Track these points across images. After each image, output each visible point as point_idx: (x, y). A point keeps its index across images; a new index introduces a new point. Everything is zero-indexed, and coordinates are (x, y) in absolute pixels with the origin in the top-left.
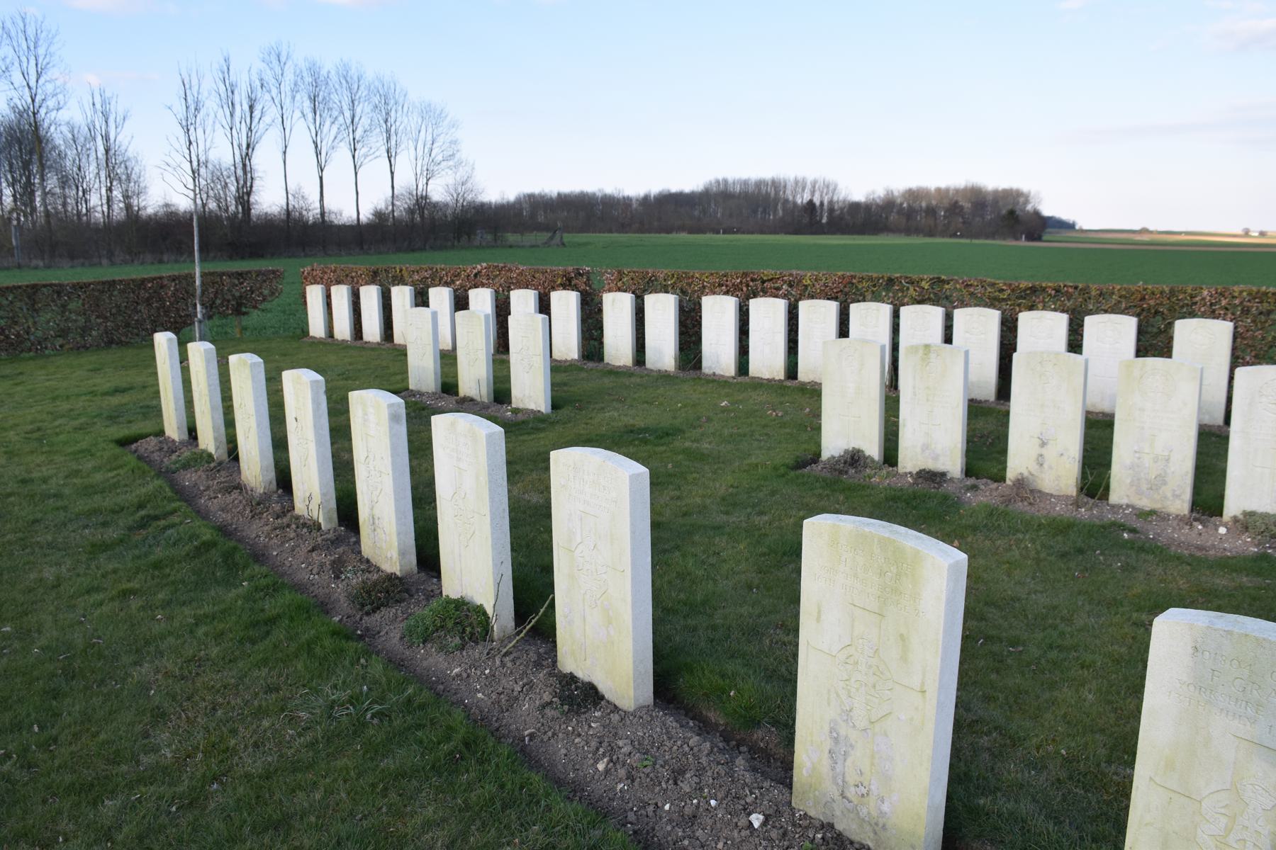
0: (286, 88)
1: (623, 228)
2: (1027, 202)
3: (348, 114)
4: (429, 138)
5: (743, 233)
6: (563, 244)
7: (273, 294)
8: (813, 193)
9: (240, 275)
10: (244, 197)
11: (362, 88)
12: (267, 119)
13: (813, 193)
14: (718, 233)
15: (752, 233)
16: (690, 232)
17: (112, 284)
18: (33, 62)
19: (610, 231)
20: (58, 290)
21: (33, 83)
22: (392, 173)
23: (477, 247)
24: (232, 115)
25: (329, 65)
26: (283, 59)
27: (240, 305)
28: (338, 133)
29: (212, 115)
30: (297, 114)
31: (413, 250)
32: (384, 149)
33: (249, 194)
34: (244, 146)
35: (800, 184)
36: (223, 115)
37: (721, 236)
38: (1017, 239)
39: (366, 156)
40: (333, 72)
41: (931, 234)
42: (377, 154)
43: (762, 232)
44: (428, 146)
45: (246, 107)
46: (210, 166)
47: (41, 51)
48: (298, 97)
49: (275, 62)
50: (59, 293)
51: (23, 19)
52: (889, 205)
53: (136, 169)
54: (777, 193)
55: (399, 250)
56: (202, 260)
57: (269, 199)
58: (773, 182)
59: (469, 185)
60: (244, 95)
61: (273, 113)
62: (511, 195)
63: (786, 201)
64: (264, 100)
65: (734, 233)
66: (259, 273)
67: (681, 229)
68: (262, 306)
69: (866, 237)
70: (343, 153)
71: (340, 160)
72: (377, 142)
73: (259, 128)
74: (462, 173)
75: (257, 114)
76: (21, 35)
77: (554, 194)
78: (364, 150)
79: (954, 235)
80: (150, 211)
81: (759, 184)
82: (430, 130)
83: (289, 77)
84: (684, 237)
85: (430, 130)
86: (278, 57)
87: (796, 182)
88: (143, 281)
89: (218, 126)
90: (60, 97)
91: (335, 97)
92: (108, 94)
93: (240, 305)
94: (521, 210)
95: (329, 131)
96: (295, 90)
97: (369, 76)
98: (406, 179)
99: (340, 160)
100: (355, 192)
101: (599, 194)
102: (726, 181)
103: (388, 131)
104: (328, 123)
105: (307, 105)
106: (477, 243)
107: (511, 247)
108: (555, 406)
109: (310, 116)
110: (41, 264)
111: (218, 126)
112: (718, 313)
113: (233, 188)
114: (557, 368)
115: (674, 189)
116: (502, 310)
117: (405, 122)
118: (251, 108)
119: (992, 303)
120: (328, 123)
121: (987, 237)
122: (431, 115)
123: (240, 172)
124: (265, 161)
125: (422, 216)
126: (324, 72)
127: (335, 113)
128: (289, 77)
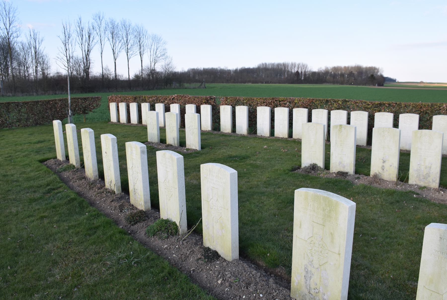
0: (102, 29)
1: (228, 81)
2: (378, 72)
3: (125, 39)
4: (156, 48)
5: (272, 83)
6: (205, 87)
7: (97, 106)
8: (298, 68)
9: (85, 99)
10: (87, 70)
11: (130, 29)
12: (95, 41)
13: (298, 68)
14: (263, 83)
15: (276, 83)
16: (253, 83)
17: (38, 102)
18: (8, 20)
19: (223, 83)
20: (17, 104)
21: (8, 27)
22: (142, 61)
23: (173, 89)
24: (82, 39)
25: (118, 20)
26: (101, 18)
27: (85, 110)
28: (121, 46)
29: (75, 39)
30: (106, 39)
31: (149, 90)
32: (139, 52)
33: (88, 69)
34: (87, 51)
35: (293, 65)
36: (79, 39)
37: (264, 84)
38: (374, 85)
39: (132, 55)
40: (120, 23)
41: (342, 83)
42: (136, 54)
43: (279, 83)
44: (155, 51)
45: (87, 36)
46: (74, 58)
47: (11, 15)
48: (107, 33)
49: (98, 19)
50: (17, 106)
51: (4, 4)
52: (327, 73)
53: (46, 59)
54: (285, 68)
55: (144, 89)
56: (71, 93)
57: (96, 71)
58: (284, 64)
59: (170, 65)
60: (87, 32)
61: (97, 38)
62: (186, 70)
63: (288, 71)
64: (94, 34)
65: (269, 83)
66: (92, 98)
67: (249, 82)
68: (93, 111)
69: (318, 85)
70: (124, 53)
71: (122, 56)
72: (136, 49)
73: (92, 44)
74: (168, 61)
75: (91, 39)
76: (3, 9)
77: (202, 69)
78: (131, 52)
79: (351, 84)
80: (51, 75)
81: (278, 65)
82: (156, 45)
83: (103, 25)
84: (250, 84)
85: (156, 45)
86: (99, 18)
87: (292, 64)
88: (49, 101)
89: (77, 43)
90: (18, 33)
91: (120, 33)
92: (36, 31)
93: (85, 110)
94: (190, 74)
95: (118, 45)
96: (105, 30)
97: (133, 25)
98: (147, 63)
99: (122, 56)
100: (128, 68)
101: (219, 69)
102: (266, 64)
103: (140, 45)
104: (118, 42)
105: (110, 35)
106: (173, 87)
107: (186, 88)
108: (202, 148)
109: (111, 40)
110: (11, 95)
111: (77, 43)
112: (263, 113)
113: (82, 67)
114: (203, 134)
115: (247, 67)
116: (183, 112)
117: (146, 42)
118: (89, 36)
119: (365, 109)
120: (118, 42)
121: (363, 85)
122: (156, 39)
123: (85, 61)
124: (94, 56)
125: (153, 77)
126: (116, 23)
127: (120, 39)
128: (103, 25)
